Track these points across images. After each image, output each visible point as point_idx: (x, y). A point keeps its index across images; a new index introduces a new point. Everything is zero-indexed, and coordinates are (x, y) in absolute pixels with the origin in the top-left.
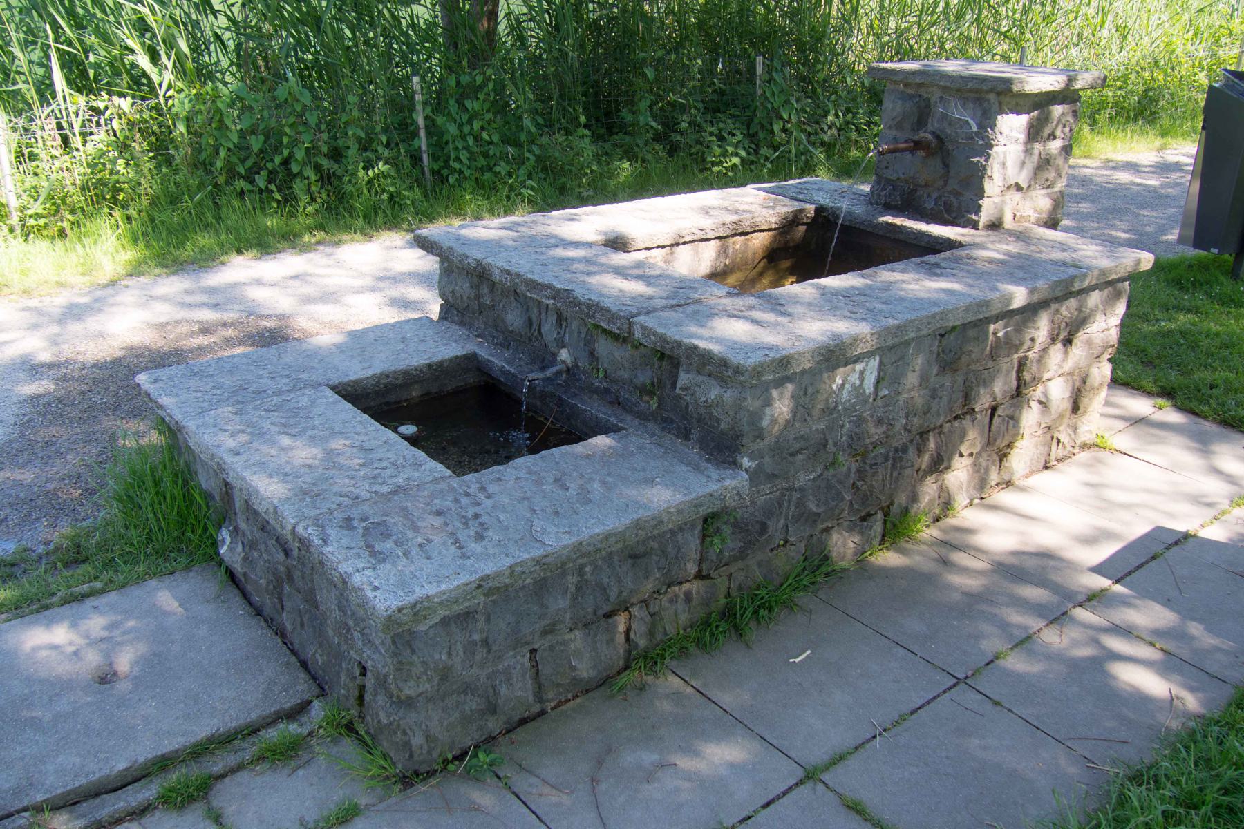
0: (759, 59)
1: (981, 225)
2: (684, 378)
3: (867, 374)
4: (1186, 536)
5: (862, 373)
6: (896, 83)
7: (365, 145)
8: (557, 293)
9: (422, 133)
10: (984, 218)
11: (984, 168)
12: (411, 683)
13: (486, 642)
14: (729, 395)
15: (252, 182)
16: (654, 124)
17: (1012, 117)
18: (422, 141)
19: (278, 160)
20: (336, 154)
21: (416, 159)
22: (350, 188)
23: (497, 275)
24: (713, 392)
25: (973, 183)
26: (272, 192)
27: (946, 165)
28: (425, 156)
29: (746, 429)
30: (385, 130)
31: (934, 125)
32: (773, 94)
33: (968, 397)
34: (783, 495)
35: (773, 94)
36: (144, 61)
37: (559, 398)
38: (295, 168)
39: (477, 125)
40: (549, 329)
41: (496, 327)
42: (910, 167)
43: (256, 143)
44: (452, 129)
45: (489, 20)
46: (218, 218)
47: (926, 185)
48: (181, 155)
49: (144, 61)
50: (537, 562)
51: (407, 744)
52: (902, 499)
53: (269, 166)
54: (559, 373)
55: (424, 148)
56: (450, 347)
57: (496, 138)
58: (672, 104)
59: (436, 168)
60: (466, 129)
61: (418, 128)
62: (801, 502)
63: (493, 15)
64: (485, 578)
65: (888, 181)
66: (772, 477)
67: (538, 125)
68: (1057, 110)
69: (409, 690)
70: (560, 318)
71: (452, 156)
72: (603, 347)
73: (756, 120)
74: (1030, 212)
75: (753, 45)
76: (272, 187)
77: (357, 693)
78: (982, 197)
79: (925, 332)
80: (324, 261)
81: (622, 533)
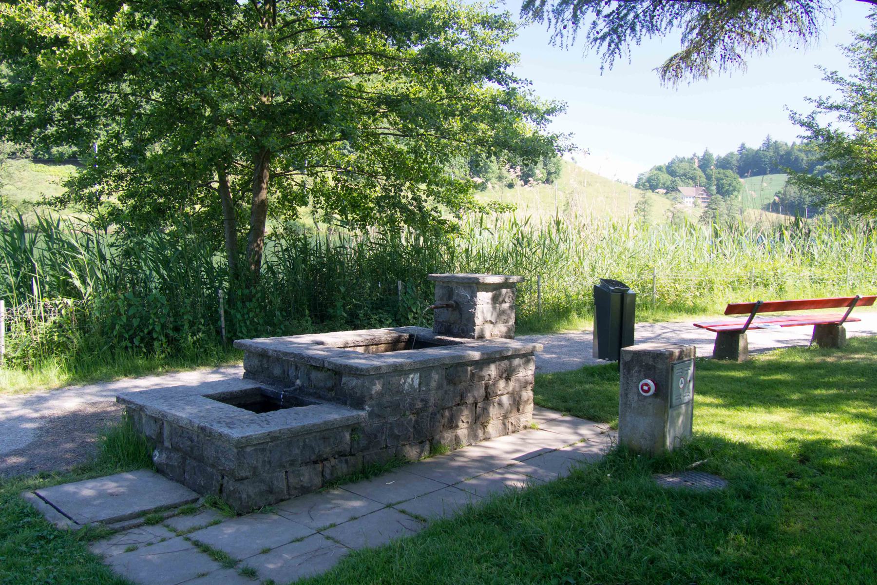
0: (400, 282)
1: (476, 337)
2: (344, 380)
3: (415, 380)
4: (555, 450)
5: (412, 379)
6: (439, 281)
7: (192, 324)
8: (295, 355)
9: (223, 319)
10: (476, 334)
11: (474, 313)
12: (243, 471)
13: (269, 462)
14: (360, 382)
15: (132, 342)
16: (345, 315)
17: (484, 293)
18: (223, 323)
19: (146, 331)
20: (177, 329)
21: (218, 332)
22: (184, 345)
23: (270, 353)
24: (354, 382)
25: (470, 320)
26: (142, 347)
27: (461, 314)
28: (224, 331)
29: (366, 394)
30: (203, 317)
31: (455, 298)
32: (408, 300)
33: (462, 397)
34: (383, 425)
35: (408, 300)
36: (78, 283)
37: (296, 398)
38: (155, 335)
39: (251, 314)
40: (292, 372)
41: (269, 377)
42: (446, 315)
43: (136, 322)
44: (239, 316)
45: (256, 265)
46: (113, 359)
47: (454, 323)
48: (95, 328)
49: (78, 283)
50: (289, 430)
51: (240, 498)
52: (437, 437)
53: (142, 334)
54: (296, 389)
55: (223, 326)
56: (250, 385)
57: (261, 321)
58: (355, 305)
59: (229, 336)
60: (246, 317)
61: (220, 316)
62: (391, 429)
63: (258, 263)
64: (271, 432)
65: (440, 322)
66: (379, 416)
67: (283, 316)
68: (504, 291)
69: (243, 474)
70: (297, 367)
71: (238, 330)
72: (314, 375)
73: (399, 313)
74: (498, 333)
75: (397, 275)
76: (142, 345)
77: (219, 488)
78: (475, 326)
79: (436, 364)
80: (171, 379)
81: (319, 425)
